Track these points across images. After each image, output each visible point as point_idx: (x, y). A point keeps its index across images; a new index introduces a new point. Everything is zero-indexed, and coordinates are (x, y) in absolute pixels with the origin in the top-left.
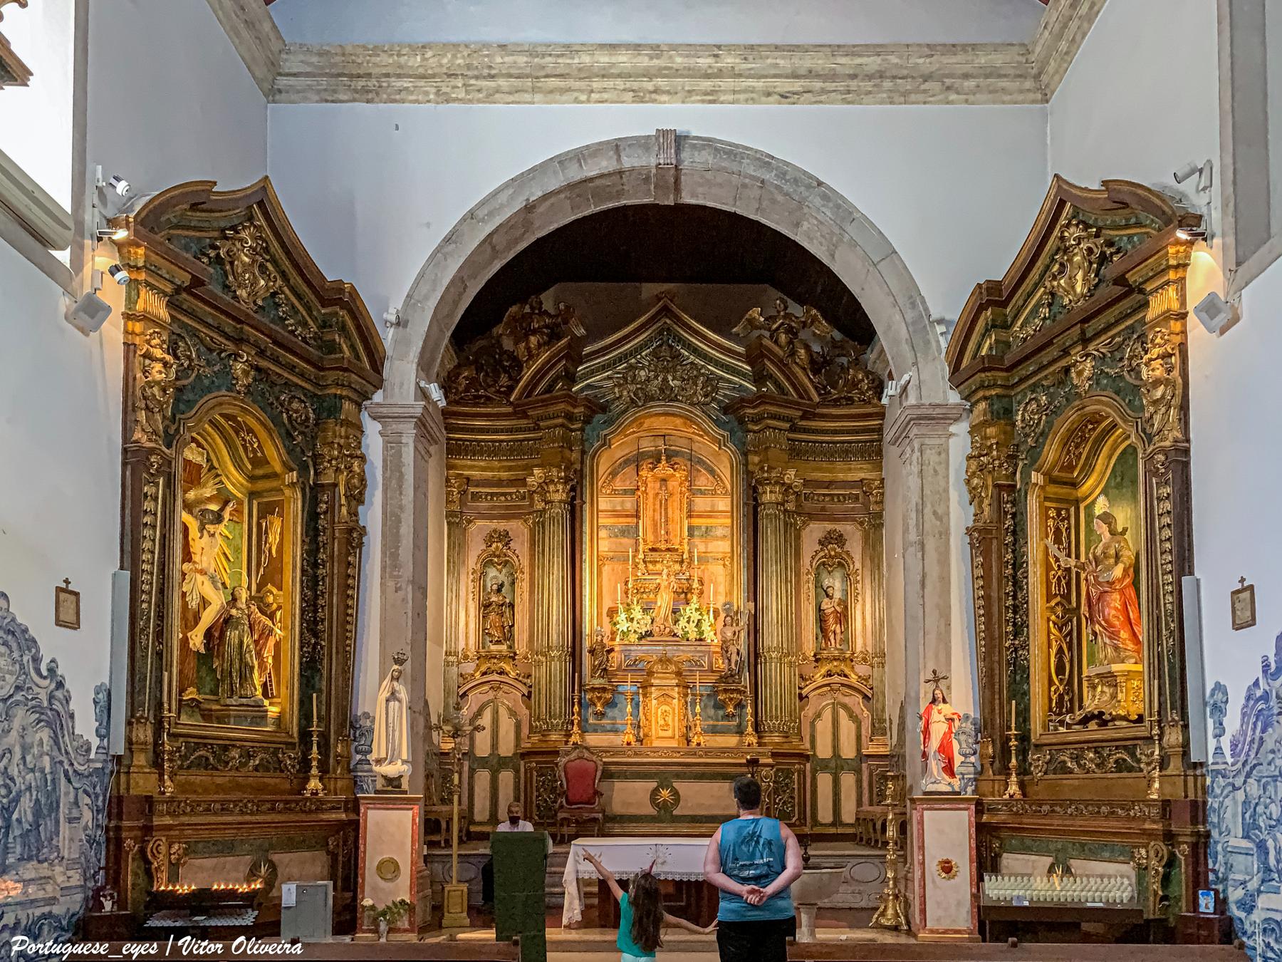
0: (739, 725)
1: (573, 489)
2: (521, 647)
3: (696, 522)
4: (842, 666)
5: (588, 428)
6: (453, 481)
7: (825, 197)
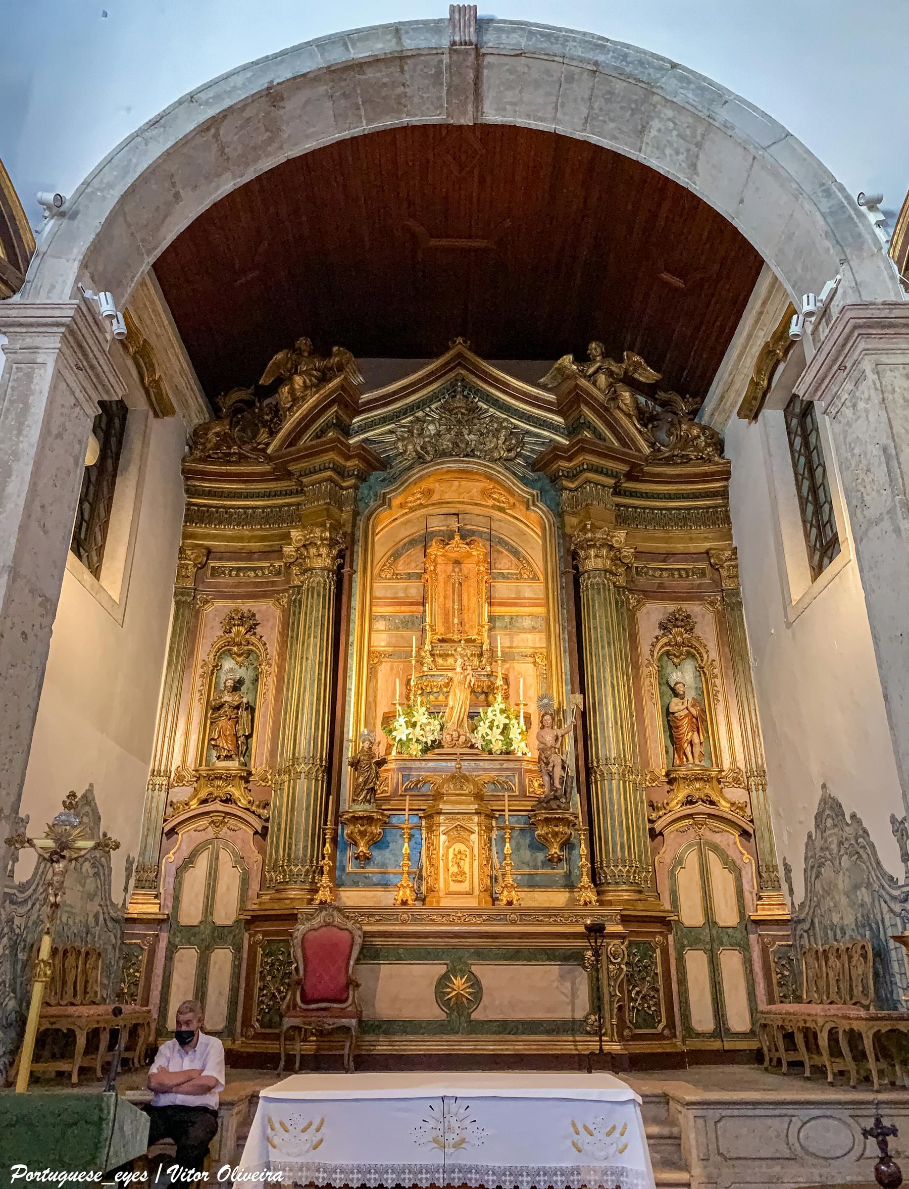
0: (568, 875)
1: (341, 555)
2: (259, 763)
3: (498, 610)
4: (708, 790)
5: (363, 487)
6: (189, 552)
7: (682, 79)
